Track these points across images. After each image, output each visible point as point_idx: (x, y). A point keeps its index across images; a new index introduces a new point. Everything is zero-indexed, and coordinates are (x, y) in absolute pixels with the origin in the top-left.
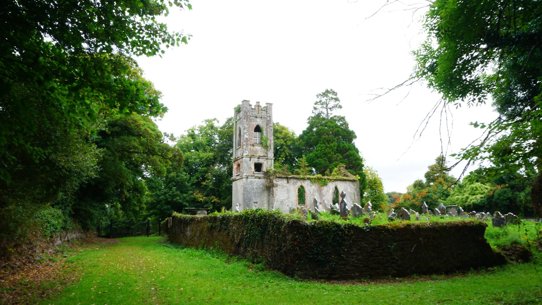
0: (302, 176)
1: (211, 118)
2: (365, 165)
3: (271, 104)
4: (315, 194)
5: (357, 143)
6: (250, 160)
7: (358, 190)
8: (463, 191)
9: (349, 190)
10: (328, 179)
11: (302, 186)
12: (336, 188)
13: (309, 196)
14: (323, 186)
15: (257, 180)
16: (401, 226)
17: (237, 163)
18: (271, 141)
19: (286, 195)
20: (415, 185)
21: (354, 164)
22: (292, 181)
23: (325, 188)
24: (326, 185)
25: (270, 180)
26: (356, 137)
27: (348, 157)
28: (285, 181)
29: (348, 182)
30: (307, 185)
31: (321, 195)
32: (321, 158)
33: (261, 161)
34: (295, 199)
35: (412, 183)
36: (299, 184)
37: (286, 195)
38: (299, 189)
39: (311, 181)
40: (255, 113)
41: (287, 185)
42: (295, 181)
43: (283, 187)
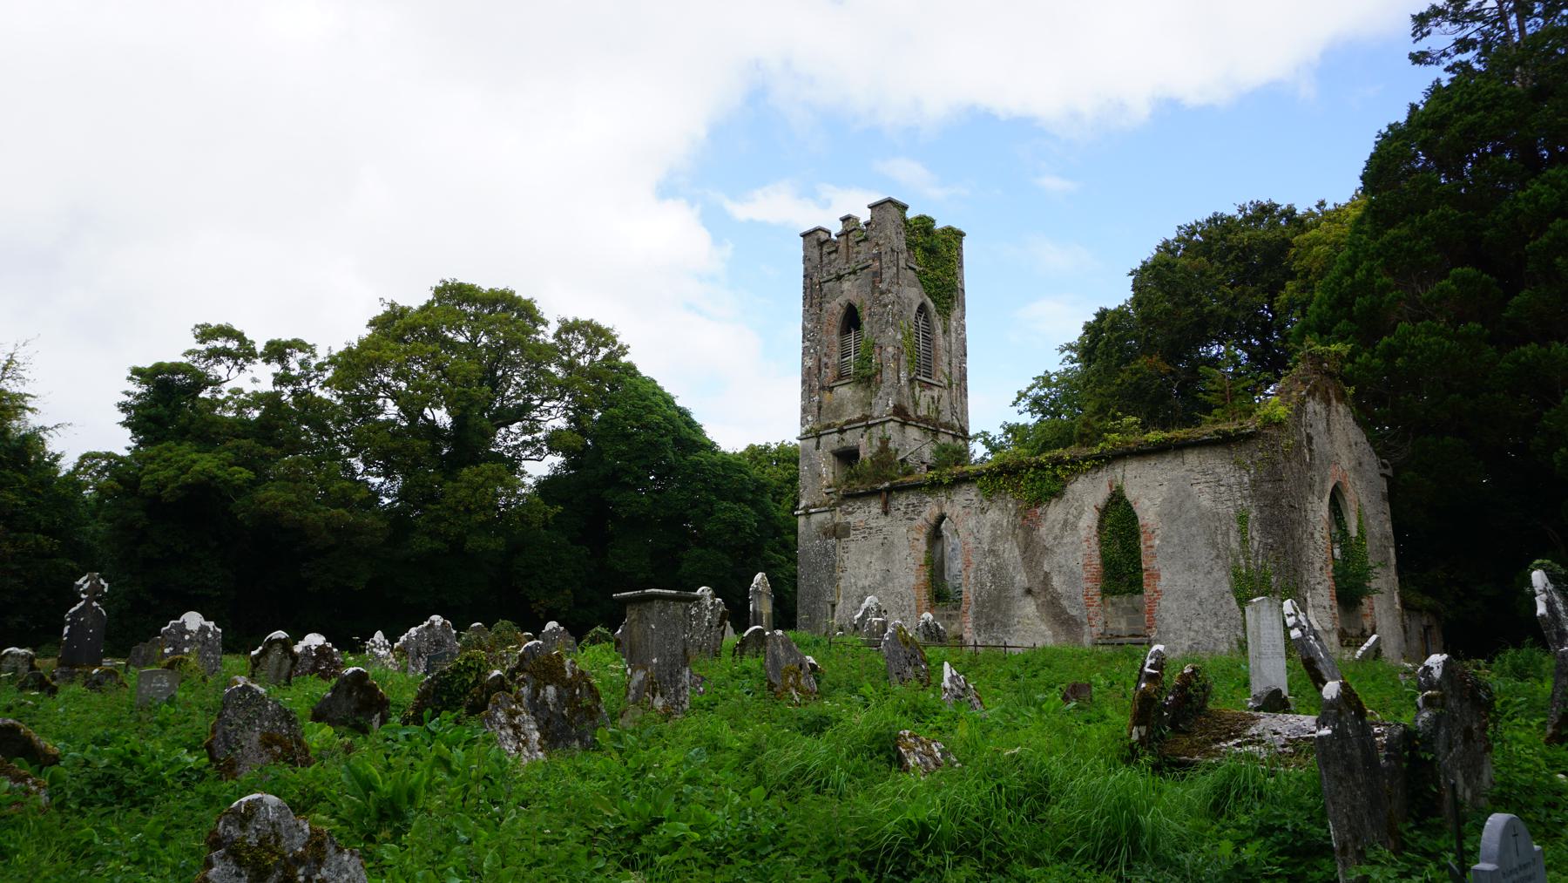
3: (961, 235)
4: (1000, 546)
6: (818, 447)
9: (1206, 501)
12: (935, 534)
14: (1038, 502)
22: (901, 501)
23: (1055, 512)
24: (1058, 494)
28: (875, 507)
29: (1192, 458)
31: (1032, 551)
33: (851, 438)
41: (882, 522)
42: (913, 499)
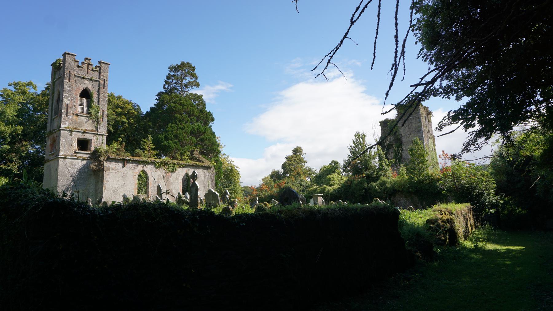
0: (144, 159)
1: (24, 80)
2: (222, 152)
4: (160, 181)
5: (215, 127)
7: (213, 178)
8: (320, 182)
10: (178, 164)
11: (143, 171)
13: (153, 184)
15: (80, 161)
16: (491, 249)
17: (51, 137)
18: (104, 108)
19: (121, 182)
20: (272, 176)
21: (209, 147)
25: (100, 161)
26: (213, 120)
27: (202, 140)
30: (149, 169)
31: (167, 182)
32: (171, 140)
33: (87, 136)
34: (133, 187)
35: (268, 174)
36: (140, 168)
37: (121, 182)
38: (140, 176)
39: (155, 166)
40: (82, 73)
43: (117, 171)
